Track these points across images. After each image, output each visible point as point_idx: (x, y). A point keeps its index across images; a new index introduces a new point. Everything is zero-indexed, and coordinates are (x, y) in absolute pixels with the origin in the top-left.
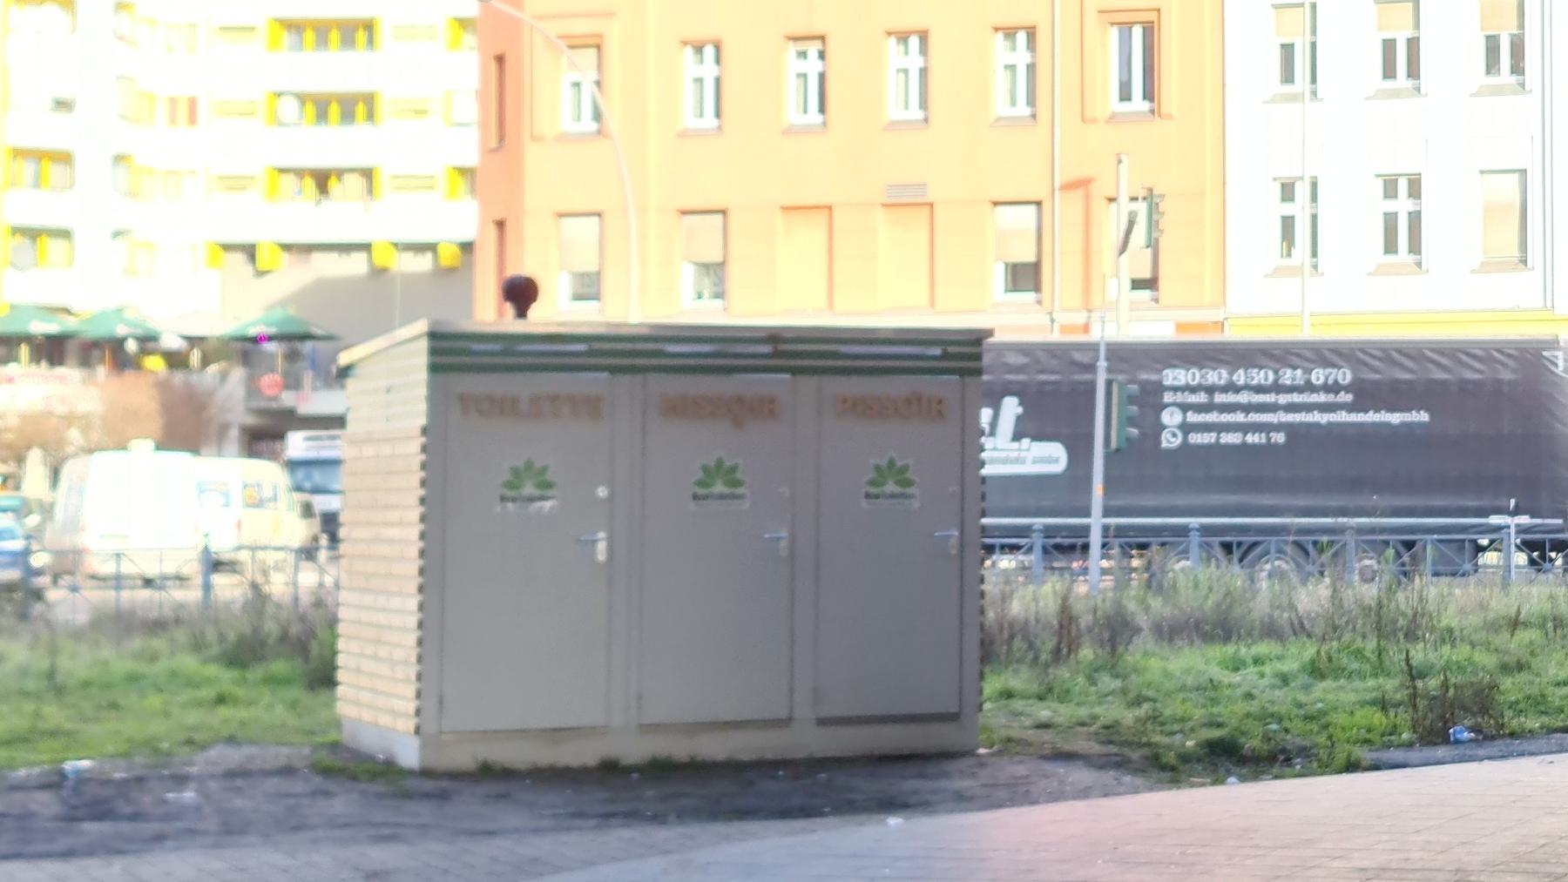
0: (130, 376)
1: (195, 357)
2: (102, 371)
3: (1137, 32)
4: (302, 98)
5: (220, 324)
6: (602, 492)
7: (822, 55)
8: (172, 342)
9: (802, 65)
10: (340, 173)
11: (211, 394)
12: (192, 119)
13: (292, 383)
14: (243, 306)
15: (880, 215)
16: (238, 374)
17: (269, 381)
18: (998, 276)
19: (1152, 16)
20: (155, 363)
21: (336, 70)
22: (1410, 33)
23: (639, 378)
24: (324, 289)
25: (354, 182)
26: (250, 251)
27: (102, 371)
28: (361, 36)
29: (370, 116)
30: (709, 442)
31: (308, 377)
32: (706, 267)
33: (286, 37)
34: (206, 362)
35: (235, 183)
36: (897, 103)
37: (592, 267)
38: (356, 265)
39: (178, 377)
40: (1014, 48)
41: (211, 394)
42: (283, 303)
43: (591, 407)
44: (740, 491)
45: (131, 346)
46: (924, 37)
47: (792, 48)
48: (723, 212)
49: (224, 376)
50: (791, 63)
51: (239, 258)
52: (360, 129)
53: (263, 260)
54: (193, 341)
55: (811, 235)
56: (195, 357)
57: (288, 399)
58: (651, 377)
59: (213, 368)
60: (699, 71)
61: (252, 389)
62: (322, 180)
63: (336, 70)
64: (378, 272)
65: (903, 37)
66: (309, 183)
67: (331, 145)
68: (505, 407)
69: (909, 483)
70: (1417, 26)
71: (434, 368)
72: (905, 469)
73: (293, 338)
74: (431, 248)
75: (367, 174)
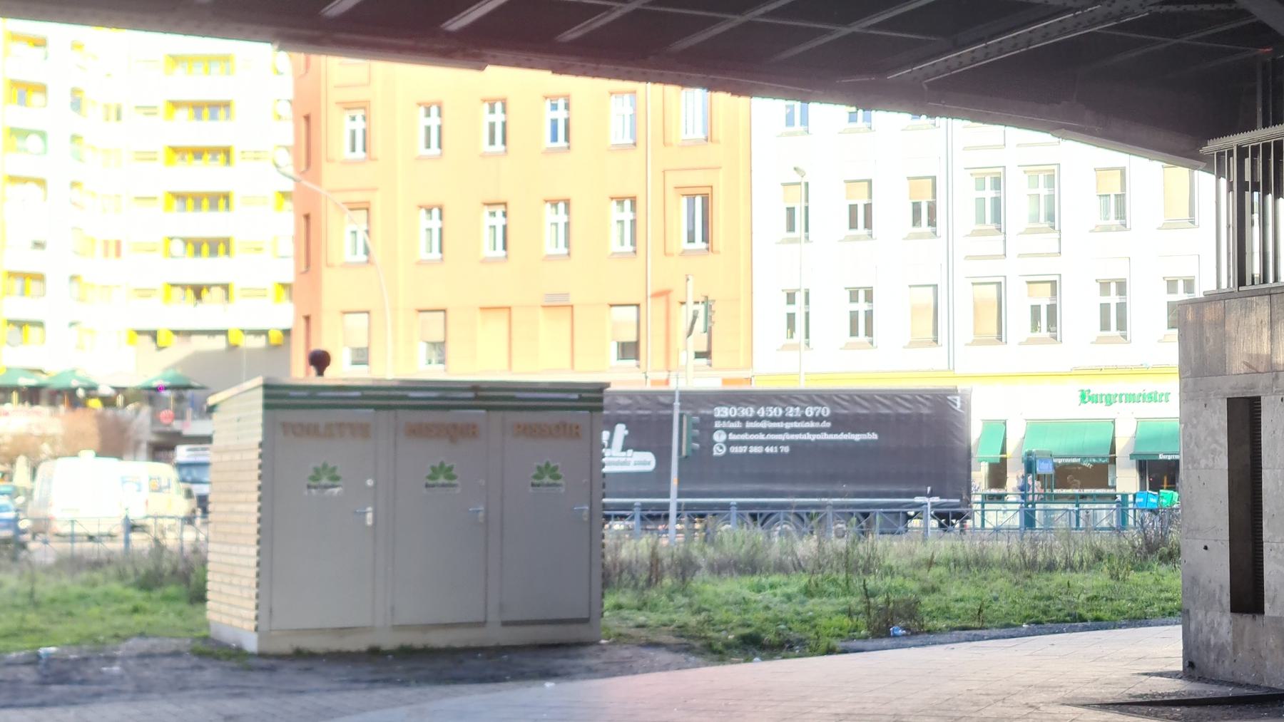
0: (80, 411)
1: (120, 400)
2: (62, 408)
3: (698, 200)
4: (186, 241)
5: (135, 379)
6: (370, 482)
7: (505, 214)
8: (105, 390)
9: (493, 221)
10: (209, 287)
11: (130, 422)
12: (118, 254)
13: (180, 416)
14: (149, 369)
15: (541, 312)
16: (146, 410)
17: (165, 414)
18: (613, 350)
19: (707, 191)
20: (95, 404)
21: (207, 224)
22: (866, 201)
23: (392, 413)
25: (218, 293)
26: (154, 335)
27: (62, 408)
28: (222, 203)
29: (227, 252)
30: (435, 452)
31: (189, 412)
33: (175, 204)
34: (126, 403)
35: (145, 293)
36: (551, 244)
37: (364, 344)
38: (219, 343)
39: (110, 412)
40: (623, 210)
41: (130, 422)
42: (174, 366)
43: (363, 431)
44: (454, 482)
45: (81, 393)
46: (567, 203)
47: (487, 210)
48: (444, 311)
49: (137, 411)
50: (486, 220)
51: (147, 339)
52: (221, 259)
53: (162, 340)
54: (119, 390)
55: (497, 325)
56: (120, 400)
57: (177, 425)
58: (400, 412)
59: (131, 407)
60: (430, 224)
61: (155, 419)
62: (198, 291)
63: (207, 224)
64: (232, 348)
65: (555, 204)
66: (190, 293)
68: (310, 431)
69: (558, 477)
70: (870, 197)
71: (267, 407)
72: (555, 468)
73: (180, 388)
74: (264, 332)
75: (226, 287)
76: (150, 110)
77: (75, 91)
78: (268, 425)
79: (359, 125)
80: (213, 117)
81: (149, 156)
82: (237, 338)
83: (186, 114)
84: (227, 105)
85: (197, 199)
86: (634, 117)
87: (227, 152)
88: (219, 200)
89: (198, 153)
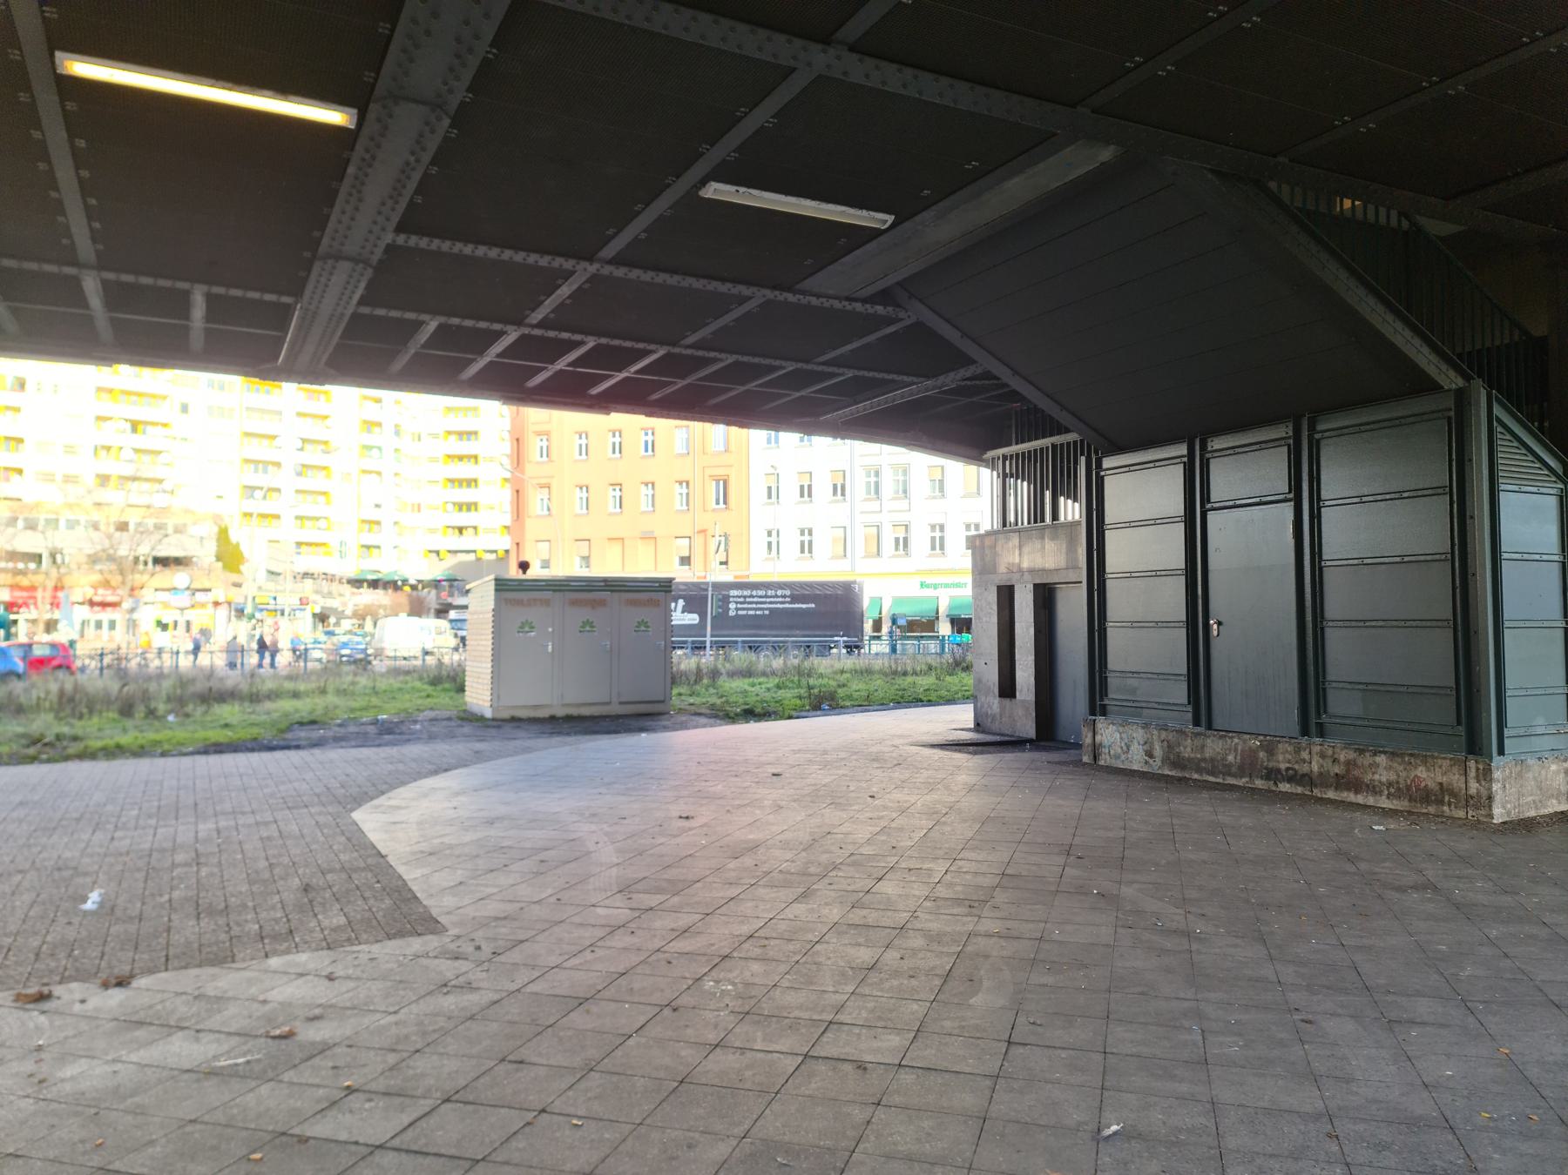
5: (428, 577)
8: (412, 582)
13: (451, 595)
16: (434, 592)
17: (444, 594)
18: (677, 560)
20: (407, 588)
21: (465, 495)
24: (461, 564)
25: (471, 531)
26: (437, 553)
35: (433, 531)
36: (645, 505)
38: (472, 557)
41: (161, 668)
43: (547, 603)
55: (617, 548)
57: (450, 600)
61: (438, 597)
62: (461, 530)
63: (465, 495)
64: (479, 559)
67: (463, 519)
73: (451, 580)
78: (497, 600)
79: (545, 444)
83: (455, 437)
85: (460, 482)
87: (476, 457)
88: (471, 482)
89: (461, 458)
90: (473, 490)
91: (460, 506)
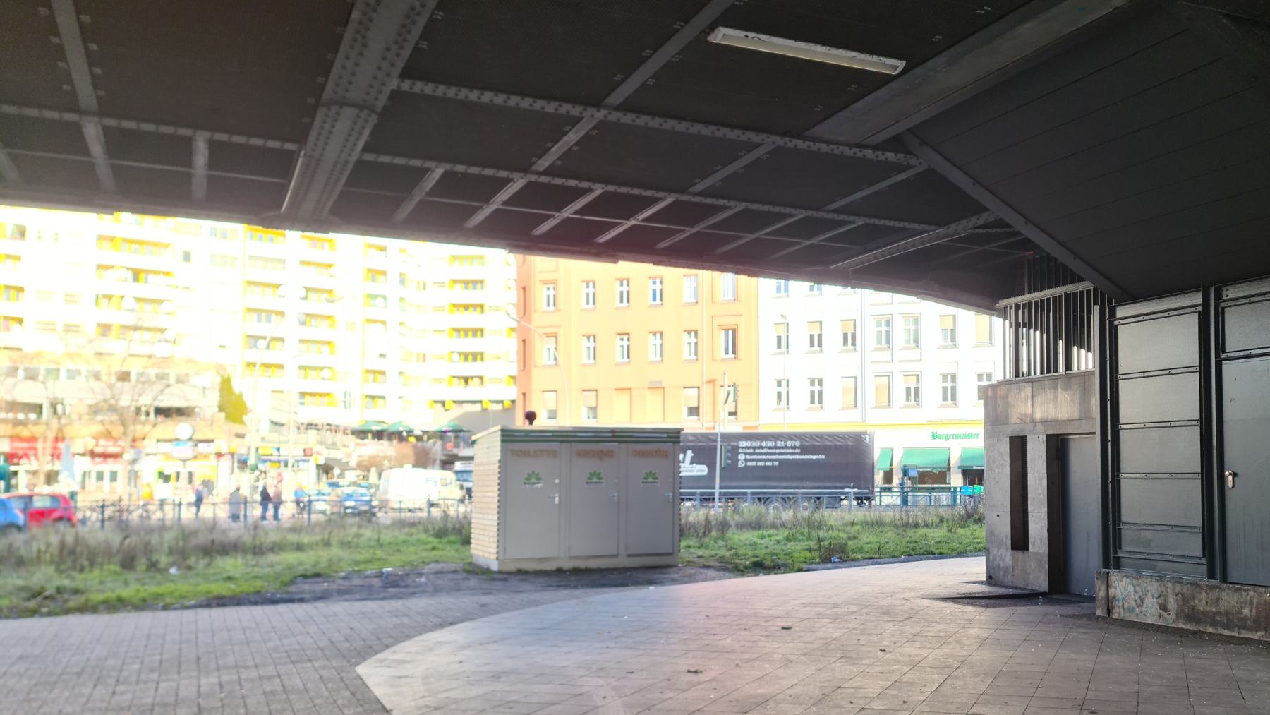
1: (425, 438)
2: (395, 442)
4: (460, 354)
8: (418, 432)
13: (457, 446)
16: (439, 443)
17: (449, 445)
18: (686, 411)
20: (412, 439)
21: (471, 344)
25: (477, 381)
26: (443, 403)
27: (395, 442)
32: (591, 408)
33: (454, 334)
34: (429, 439)
36: (653, 355)
38: (477, 407)
39: (420, 444)
43: (554, 454)
45: (405, 434)
51: (440, 405)
54: (425, 432)
55: (625, 398)
56: (425, 438)
57: (455, 451)
61: (444, 448)
62: (466, 380)
63: (471, 344)
64: (485, 410)
66: (462, 381)
67: (470, 369)
71: (503, 441)
73: (457, 431)
74: (502, 402)
75: (481, 378)
76: (441, 285)
77: (401, 274)
79: (551, 293)
80: (474, 288)
81: (440, 309)
82: (487, 405)
83: (460, 286)
84: (482, 282)
86: (696, 288)
87: (482, 306)
88: (477, 332)
89: (466, 307)
90: (478, 340)
91: (466, 356)
